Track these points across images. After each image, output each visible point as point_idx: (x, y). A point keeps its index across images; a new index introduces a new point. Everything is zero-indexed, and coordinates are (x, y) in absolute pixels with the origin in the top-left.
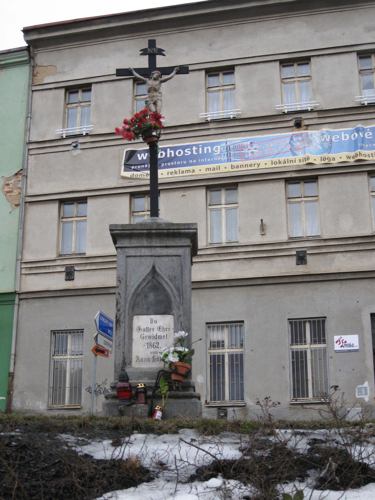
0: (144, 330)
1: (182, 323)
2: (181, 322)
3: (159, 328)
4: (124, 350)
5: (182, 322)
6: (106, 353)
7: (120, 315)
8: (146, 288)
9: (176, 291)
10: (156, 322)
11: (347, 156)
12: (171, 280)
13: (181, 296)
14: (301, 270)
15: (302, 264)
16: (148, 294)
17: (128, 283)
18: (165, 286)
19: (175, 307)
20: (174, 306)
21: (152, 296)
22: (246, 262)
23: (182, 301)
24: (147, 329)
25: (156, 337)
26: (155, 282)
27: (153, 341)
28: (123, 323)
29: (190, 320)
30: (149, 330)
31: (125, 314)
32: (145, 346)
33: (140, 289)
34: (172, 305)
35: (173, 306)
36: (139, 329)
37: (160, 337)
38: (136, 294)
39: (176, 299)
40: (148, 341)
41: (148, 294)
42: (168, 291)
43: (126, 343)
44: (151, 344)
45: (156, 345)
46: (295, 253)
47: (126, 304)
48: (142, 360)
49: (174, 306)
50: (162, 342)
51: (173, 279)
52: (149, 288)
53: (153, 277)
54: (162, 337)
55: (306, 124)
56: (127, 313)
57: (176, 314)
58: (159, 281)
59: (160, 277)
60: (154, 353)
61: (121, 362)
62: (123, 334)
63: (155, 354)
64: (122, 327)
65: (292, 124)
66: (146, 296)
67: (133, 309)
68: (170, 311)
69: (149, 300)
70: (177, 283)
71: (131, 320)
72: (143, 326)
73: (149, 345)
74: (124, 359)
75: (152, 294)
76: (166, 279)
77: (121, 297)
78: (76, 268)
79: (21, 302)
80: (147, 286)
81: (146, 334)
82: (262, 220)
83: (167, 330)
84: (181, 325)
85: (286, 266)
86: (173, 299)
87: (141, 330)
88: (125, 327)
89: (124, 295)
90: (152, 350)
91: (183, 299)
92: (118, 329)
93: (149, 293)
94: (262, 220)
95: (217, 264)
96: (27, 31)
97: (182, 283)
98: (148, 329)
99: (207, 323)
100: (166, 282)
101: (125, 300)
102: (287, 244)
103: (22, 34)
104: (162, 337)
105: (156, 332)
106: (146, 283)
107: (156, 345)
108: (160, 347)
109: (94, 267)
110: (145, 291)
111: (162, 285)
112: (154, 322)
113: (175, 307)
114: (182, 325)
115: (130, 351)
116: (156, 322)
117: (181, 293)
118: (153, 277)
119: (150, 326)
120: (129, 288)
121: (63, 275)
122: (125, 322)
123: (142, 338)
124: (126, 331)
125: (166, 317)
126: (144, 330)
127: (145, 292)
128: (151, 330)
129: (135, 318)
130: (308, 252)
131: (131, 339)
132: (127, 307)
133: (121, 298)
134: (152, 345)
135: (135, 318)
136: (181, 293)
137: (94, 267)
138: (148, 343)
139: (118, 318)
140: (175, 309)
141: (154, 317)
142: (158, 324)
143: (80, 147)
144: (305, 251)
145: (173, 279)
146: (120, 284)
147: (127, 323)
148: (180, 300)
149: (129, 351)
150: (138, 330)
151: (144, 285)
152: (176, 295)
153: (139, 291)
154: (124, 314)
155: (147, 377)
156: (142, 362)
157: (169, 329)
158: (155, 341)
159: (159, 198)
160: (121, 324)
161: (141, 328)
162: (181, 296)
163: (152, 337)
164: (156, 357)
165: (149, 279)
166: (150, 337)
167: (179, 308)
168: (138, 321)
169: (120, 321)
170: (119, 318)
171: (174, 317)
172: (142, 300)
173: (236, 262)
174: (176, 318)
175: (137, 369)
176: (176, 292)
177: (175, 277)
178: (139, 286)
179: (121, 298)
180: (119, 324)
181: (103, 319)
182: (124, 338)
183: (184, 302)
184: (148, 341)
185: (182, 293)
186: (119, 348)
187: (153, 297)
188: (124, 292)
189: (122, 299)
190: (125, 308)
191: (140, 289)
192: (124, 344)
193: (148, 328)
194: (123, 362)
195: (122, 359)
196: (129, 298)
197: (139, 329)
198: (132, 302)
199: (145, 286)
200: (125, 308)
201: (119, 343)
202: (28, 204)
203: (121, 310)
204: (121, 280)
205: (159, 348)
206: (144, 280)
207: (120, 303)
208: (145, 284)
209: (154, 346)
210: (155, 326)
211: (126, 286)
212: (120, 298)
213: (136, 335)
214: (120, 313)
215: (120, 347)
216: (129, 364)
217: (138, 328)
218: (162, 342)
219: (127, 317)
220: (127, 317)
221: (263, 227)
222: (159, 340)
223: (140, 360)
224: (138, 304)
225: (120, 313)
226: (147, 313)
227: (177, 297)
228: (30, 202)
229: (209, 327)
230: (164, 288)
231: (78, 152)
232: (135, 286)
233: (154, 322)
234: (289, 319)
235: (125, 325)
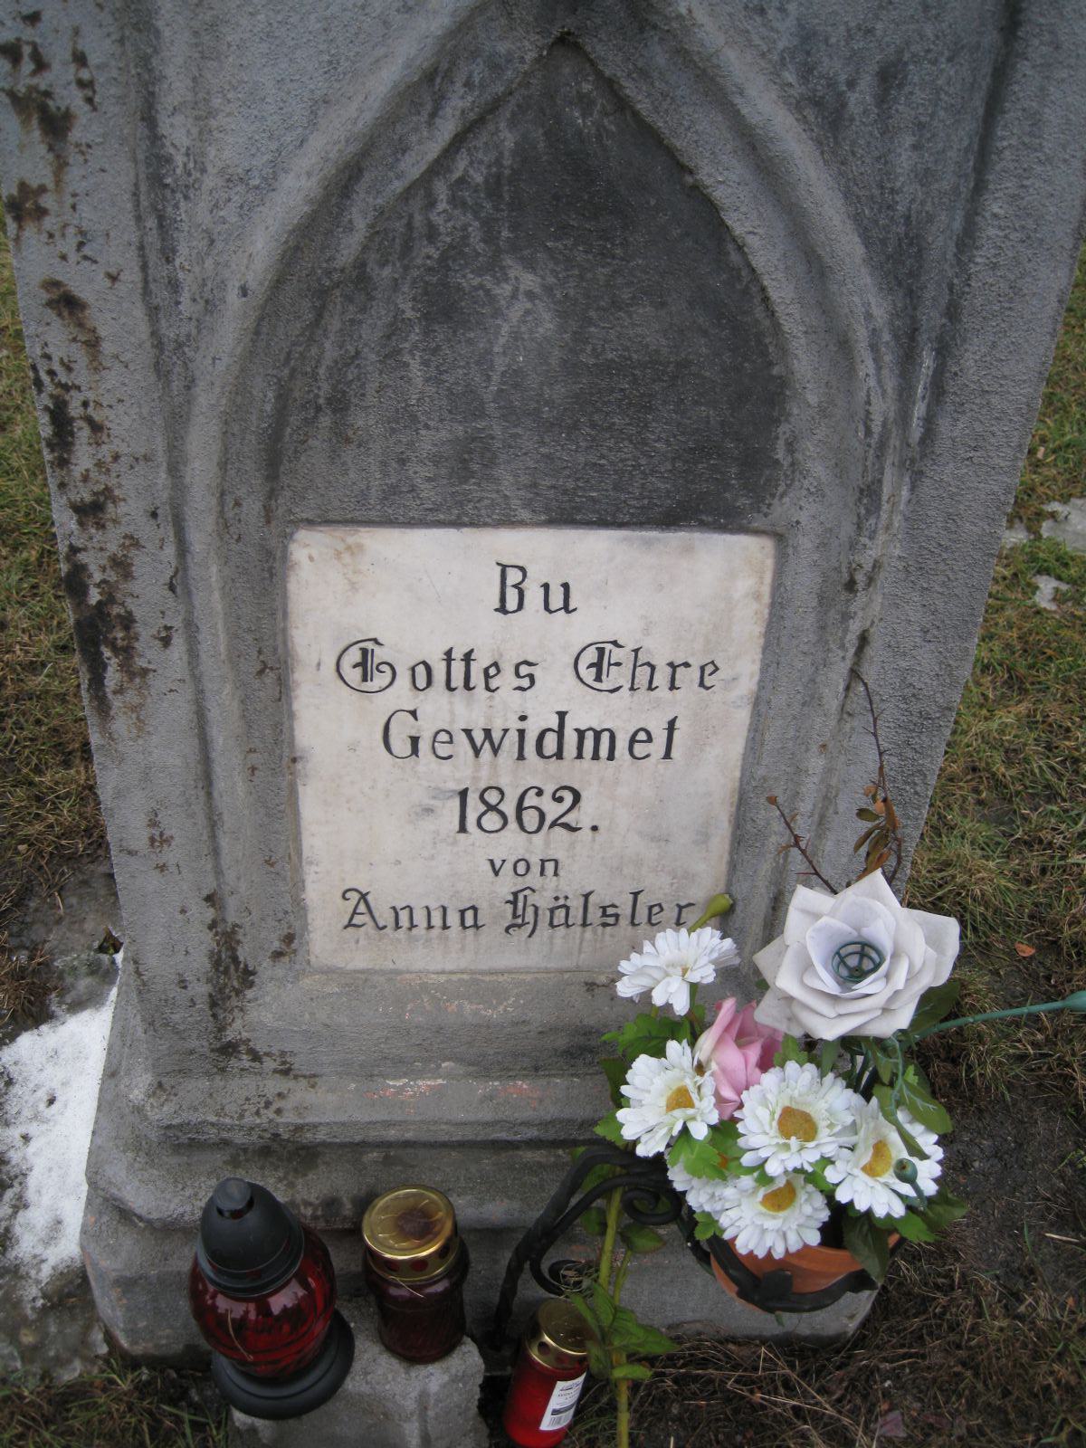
0: (422, 677)
1: (875, 651)
2: (864, 640)
3: (590, 656)
4: (218, 872)
7: (121, 565)
8: (441, 189)
9: (866, 279)
10: (562, 600)
12: (826, 114)
13: (928, 361)
16: (470, 280)
17: (177, 132)
18: (719, 194)
19: (819, 470)
20: (809, 447)
21: (523, 310)
23: (929, 421)
24: (458, 668)
25: (555, 741)
26: (585, 103)
27: (511, 776)
28: (166, 642)
30: (477, 678)
31: (183, 549)
32: (429, 810)
33: (359, 218)
34: (784, 430)
35: (791, 448)
36: (365, 665)
37: (598, 743)
38: (312, 279)
39: (851, 371)
40: (463, 770)
41: (470, 280)
42: (758, 261)
43: (229, 821)
44: (492, 798)
45: (553, 810)
47: (176, 422)
48: (402, 918)
49: (812, 442)
50: (611, 792)
51: (860, 99)
52: (493, 188)
53: (566, 41)
54: (622, 744)
56: (200, 537)
57: (822, 546)
58: (643, 107)
59: (659, 56)
60: (522, 866)
61: (199, 962)
62: (190, 746)
63: (533, 879)
64: (157, 684)
66: (445, 308)
67: (274, 461)
68: (743, 502)
69: (484, 360)
70: (905, 160)
71: (265, 578)
72: (411, 637)
73: (474, 808)
74: (227, 939)
75: (529, 281)
76: (766, 106)
77: (93, 344)
80: (461, 165)
81: (439, 709)
83: (687, 677)
84: (855, 674)
86: (805, 364)
87: (380, 680)
88: (197, 679)
89: (139, 312)
90: (511, 843)
91: (938, 390)
92: (116, 703)
93: (493, 267)
97: (979, 188)
98: (462, 671)
100: (752, 143)
101: (160, 370)
104: (622, 744)
105: (559, 695)
106: (447, 128)
107: (553, 810)
108: (586, 823)
110: (432, 234)
111: (686, 170)
112: (534, 596)
113: (819, 470)
114: (870, 672)
115: (280, 854)
116: (562, 600)
117: (932, 318)
118: (566, 41)
119: (487, 635)
120: (195, 214)
122: (190, 626)
123: (401, 745)
124: (214, 714)
125: (688, 549)
126: (422, 677)
127: (427, 252)
128: (506, 680)
131: (276, 759)
132: (201, 470)
133: (96, 365)
134: (509, 808)
135: (314, 562)
136: (932, 318)
138: (463, 794)
139: (94, 596)
140: (819, 493)
141: (543, 550)
142: (584, 628)
145: (860, 99)
146: (61, 165)
147: (215, 639)
148: (905, 395)
149: (270, 863)
150: (354, 676)
151: (413, 166)
152: (861, 334)
153: (349, 248)
154: (170, 551)
155: (458, 1059)
156: (401, 934)
157: (708, 670)
158: (536, 772)
159: (651, 1155)
160: (147, 652)
161: (380, 654)
162: (928, 361)
163: (513, 737)
164: (544, 901)
165: (495, 67)
166: (486, 742)
167: (870, 494)
168: (353, 586)
169: (128, 621)
170: (110, 599)
171: (782, 559)
172: (391, 357)
174: (806, 582)
175: (357, 984)
176: (865, 299)
177: (890, 77)
178: (346, 180)
179: (96, 365)
180: (126, 653)
182: (207, 780)
183: (944, 425)
184: (463, 770)
185: (952, 312)
186: (162, 868)
187: (547, 324)
188: (132, 276)
189: (112, 378)
190: (174, 470)
191: (359, 218)
192: (213, 823)
193: (468, 658)
194: (217, 963)
195: (201, 944)
196: (226, 337)
197: (363, 664)
198: (264, 397)
199: (439, 167)
200: (174, 470)
201: (153, 823)
203: (130, 511)
204: (71, 99)
205: (586, 833)
206: (427, 87)
207: (96, 427)
208: (433, 149)
209: (531, 819)
210: (551, 639)
211: (159, 183)
212: (80, 356)
213: (327, 720)
214: (112, 541)
215: (171, 855)
216: (278, 955)
217: (354, 655)
218: (611, 792)
219: (210, 576)
220: (210, 576)
223: (385, 917)
224: (339, 404)
225: (112, 541)
226: (459, 493)
227: (866, 366)
230: (709, 211)
232: (297, 190)
233: (534, 596)
235: (193, 654)
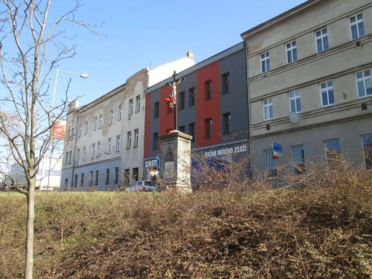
5: (360, 134)
6: (278, 158)
11: (138, 129)
14: (268, 132)
15: (365, 109)
22: (338, 112)
29: (193, 162)
46: (361, 105)
55: (362, 43)
65: (355, 45)
71: (164, 163)
78: (270, 125)
79: (252, 140)
82: (343, 93)
85: (358, 111)
94: (343, 93)
95: (326, 115)
96: (242, 35)
99: (324, 141)
102: (357, 102)
103: (241, 36)
109: (277, 123)
121: (266, 128)
129: (165, 163)
130: (367, 104)
137: (277, 123)
141: (170, 162)
143: (267, 76)
144: (366, 103)
158: (169, 170)
173: (334, 113)
181: (276, 145)
202: (251, 103)
221: (345, 96)
222: (171, 170)
228: (251, 102)
229: (361, 137)
231: (267, 78)
234: (360, 135)
